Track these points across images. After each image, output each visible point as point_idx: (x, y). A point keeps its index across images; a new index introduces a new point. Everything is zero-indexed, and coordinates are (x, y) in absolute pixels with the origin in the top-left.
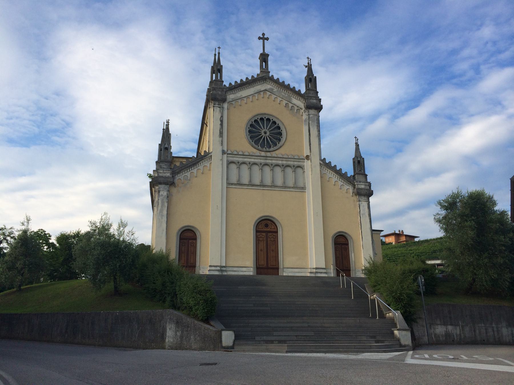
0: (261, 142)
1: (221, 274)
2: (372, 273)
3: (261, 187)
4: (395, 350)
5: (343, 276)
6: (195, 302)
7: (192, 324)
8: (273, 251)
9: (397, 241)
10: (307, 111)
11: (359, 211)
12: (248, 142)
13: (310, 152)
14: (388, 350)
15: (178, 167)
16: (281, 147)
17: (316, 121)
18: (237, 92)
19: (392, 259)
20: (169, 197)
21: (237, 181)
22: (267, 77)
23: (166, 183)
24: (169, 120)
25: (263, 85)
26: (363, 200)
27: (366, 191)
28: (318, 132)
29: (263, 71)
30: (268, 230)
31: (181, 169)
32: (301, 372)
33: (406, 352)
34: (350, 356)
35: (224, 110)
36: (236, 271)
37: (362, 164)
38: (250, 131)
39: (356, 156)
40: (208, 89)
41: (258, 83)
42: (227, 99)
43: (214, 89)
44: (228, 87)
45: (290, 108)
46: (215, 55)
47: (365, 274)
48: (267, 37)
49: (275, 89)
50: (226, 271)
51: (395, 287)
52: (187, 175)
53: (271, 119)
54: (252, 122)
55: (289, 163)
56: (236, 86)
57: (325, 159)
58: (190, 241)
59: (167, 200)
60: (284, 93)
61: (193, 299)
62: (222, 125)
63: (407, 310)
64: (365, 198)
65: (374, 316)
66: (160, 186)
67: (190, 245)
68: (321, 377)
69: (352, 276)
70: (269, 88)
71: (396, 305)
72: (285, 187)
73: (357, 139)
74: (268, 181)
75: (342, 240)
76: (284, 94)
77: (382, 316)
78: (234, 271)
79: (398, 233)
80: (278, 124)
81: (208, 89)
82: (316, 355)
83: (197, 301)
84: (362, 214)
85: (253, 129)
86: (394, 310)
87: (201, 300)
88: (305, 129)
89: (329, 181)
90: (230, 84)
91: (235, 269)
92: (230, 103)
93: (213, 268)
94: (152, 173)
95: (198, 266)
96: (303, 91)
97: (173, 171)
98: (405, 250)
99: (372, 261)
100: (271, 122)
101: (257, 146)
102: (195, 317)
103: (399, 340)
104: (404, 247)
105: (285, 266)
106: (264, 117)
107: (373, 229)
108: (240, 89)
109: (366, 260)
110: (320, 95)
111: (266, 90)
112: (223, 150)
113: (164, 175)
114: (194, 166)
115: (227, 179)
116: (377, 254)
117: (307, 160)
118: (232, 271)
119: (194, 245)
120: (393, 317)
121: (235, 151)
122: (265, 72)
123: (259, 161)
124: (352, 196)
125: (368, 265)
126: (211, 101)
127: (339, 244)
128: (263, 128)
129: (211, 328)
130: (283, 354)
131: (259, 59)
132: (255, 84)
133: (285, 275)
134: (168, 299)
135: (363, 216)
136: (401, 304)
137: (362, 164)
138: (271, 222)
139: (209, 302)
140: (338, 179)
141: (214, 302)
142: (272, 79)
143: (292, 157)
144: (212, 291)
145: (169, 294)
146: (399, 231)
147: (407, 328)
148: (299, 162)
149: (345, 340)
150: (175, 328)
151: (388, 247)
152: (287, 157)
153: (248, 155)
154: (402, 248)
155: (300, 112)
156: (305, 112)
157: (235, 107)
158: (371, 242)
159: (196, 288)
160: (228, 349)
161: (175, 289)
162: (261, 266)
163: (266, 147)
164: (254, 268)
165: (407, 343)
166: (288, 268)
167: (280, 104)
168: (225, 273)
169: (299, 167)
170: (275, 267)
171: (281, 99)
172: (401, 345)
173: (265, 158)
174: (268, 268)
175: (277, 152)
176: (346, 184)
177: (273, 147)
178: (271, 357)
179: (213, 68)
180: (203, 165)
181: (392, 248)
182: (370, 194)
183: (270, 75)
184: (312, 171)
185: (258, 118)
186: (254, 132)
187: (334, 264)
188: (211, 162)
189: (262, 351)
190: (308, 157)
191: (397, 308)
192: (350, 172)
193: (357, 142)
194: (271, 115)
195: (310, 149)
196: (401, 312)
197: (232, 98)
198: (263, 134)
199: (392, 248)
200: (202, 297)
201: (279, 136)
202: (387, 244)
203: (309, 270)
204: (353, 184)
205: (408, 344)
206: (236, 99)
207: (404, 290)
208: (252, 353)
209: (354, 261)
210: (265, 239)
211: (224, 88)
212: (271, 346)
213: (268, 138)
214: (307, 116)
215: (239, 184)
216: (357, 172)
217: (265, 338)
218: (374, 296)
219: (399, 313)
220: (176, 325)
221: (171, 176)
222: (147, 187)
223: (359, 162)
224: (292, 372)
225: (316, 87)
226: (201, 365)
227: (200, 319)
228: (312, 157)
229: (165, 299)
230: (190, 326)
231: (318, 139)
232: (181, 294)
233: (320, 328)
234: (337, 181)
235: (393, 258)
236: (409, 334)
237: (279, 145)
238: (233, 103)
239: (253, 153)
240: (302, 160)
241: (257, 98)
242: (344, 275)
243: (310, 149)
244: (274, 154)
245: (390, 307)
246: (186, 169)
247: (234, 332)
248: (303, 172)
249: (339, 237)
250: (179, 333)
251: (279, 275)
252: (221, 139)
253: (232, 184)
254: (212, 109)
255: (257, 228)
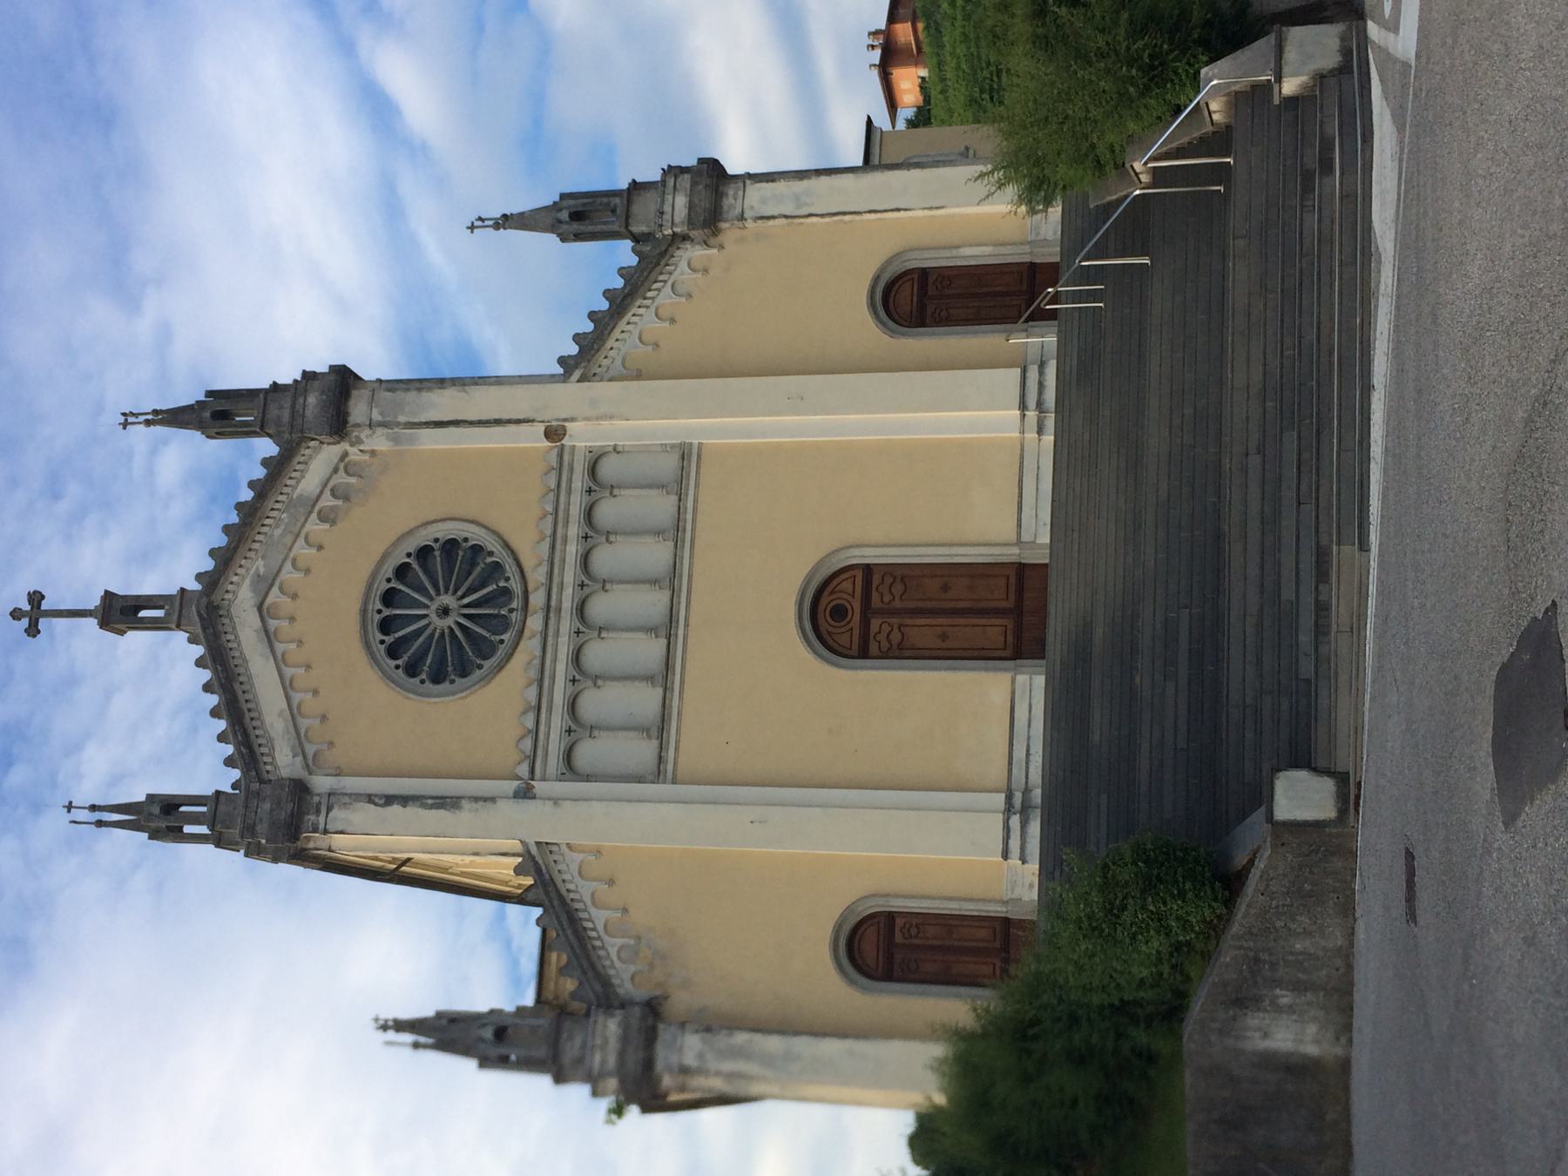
0: (484, 633)
1: (1038, 812)
2: (1044, 176)
3: (676, 635)
4: (1361, 96)
5: (1056, 299)
6: (1152, 932)
7: (1244, 943)
8: (945, 588)
9: (914, 57)
10: (354, 434)
11: (784, 221)
12: (482, 687)
13: (533, 421)
14: (1363, 126)
15: (581, 983)
16: (507, 546)
17: (399, 392)
18: (266, 731)
19: (988, 81)
20: (711, 1024)
21: (649, 737)
22: (204, 600)
23: (650, 1038)
24: (376, 1020)
25: (236, 620)
26: (740, 201)
27: (701, 187)
28: (445, 385)
29: (175, 617)
30: (857, 605)
31: (590, 974)
32: (1446, 498)
33: (1370, 51)
34: (1382, 287)
35: (344, 788)
36: (1028, 750)
37: (586, 201)
38: (438, 677)
39: (553, 226)
40: (246, 855)
41: (228, 641)
42: (295, 776)
43: (249, 829)
44: (242, 772)
45: (340, 502)
46: (100, 824)
47: (1048, 202)
48: (39, 632)
49: (254, 569)
50: (1027, 791)
51: (1102, 83)
52: (616, 949)
53: (386, 586)
54: (397, 667)
55: (576, 510)
56: (240, 738)
57: (562, 361)
58: (898, 938)
59: (724, 1032)
60: (275, 527)
61: (1140, 937)
62: (404, 800)
63: (1196, 36)
64: (731, 192)
65: (1221, 173)
66: (660, 1065)
67: (916, 941)
68: (1467, 419)
69: (1058, 259)
70: (252, 595)
71: (1176, 81)
72: (677, 531)
73: (479, 223)
74: (652, 603)
75: (906, 297)
76: (277, 526)
77: (1219, 140)
78: (1028, 754)
79: (877, 53)
80: (409, 555)
81: (246, 855)
82: (1377, 427)
83: (1148, 924)
84: (799, 207)
85: (428, 662)
86: (1198, 92)
87: (1143, 908)
88: (431, 441)
89: (657, 345)
90: (229, 762)
91: (1019, 753)
92: (310, 762)
93: (1015, 844)
94: (605, 1103)
95: (1005, 909)
96: (266, 447)
97: (599, 1006)
98: (953, 25)
99: (992, 172)
100: (401, 587)
101: (501, 651)
102: (1214, 930)
103: (1321, 78)
104: (938, 31)
105: (1013, 537)
106: (377, 617)
107: (861, 165)
108: (252, 719)
109: (988, 197)
110: (288, 375)
111: (260, 608)
112: (515, 797)
113: (613, 1044)
114: (581, 919)
115: (639, 782)
116: (967, 149)
117: (565, 434)
118: (1027, 763)
119: (914, 922)
120: (1228, 94)
121: (521, 746)
122: (180, 611)
123: (564, 640)
124: (722, 247)
125: (1011, 191)
126: (299, 844)
127: (922, 307)
128: (423, 623)
129: (1261, 864)
130: (1372, 563)
131: (122, 633)
132: (232, 653)
133: (1049, 537)
134: (1141, 1037)
135: (806, 204)
136: (1173, 61)
137: (586, 201)
138: (826, 593)
139: (1155, 872)
140: (647, 307)
141: (1153, 850)
142: (210, 581)
143: (551, 496)
144: (1107, 856)
145: (1119, 1036)
146: (873, 47)
147: (1273, 41)
148: (571, 469)
149: (1319, 298)
150: (1261, 1015)
151: (940, 96)
152: (550, 519)
153: (541, 687)
154: (944, 39)
155: (356, 463)
156: (359, 441)
157: (331, 744)
158: (916, 173)
159: (1094, 924)
160: (1348, 796)
161: (1101, 1007)
162: (1010, 639)
163: (506, 609)
164: (1016, 671)
165: (1334, 44)
166: (1019, 525)
167: (320, 548)
168: (1037, 795)
169: (593, 470)
170: (1013, 581)
171: (301, 541)
172: (1343, 70)
173: (552, 615)
174: (1018, 611)
175: (528, 562)
176: (670, 273)
177: (507, 579)
178: (1383, 619)
179: (155, 835)
180: (578, 879)
181: (943, 80)
182: (711, 173)
183: (193, 586)
184: (611, 417)
185: (382, 642)
186: (441, 662)
187: (1003, 332)
188: (564, 848)
189: (1360, 653)
190: (554, 433)
191: (1187, 76)
192: (623, 253)
193: (491, 223)
194: (370, 586)
195: (518, 422)
196: (1207, 64)
197: (291, 755)
198: (449, 622)
199: (943, 80)
200: (1130, 900)
201: (461, 553)
202: (924, 100)
203: (1031, 435)
204: (669, 246)
205: (1338, 41)
206: (295, 735)
207: (1115, 50)
208: (1368, 697)
209: (995, 245)
210: (895, 621)
211: (248, 789)
212: (1340, 614)
213: (466, 601)
214: (374, 433)
215: (660, 728)
216: (618, 223)
217: (1305, 638)
218: (1138, 171)
219: (1210, 70)
220: (1247, 1008)
221: (618, 1012)
222: (659, 1120)
223: (577, 216)
224: (1445, 536)
225: (251, 394)
226: (1412, 915)
227: (1225, 911)
228: (553, 414)
229: (1140, 1055)
230: (1251, 954)
231: (472, 387)
232: (1118, 985)
233: (1269, 404)
234: (657, 309)
235: (985, 78)
236: (1297, 35)
237: (500, 555)
238: (310, 749)
239: (529, 664)
240: (566, 458)
241: (293, 646)
242: (1050, 290)
243: (518, 422)
244: (537, 576)
245: (1186, 108)
246: (592, 953)
247: (1281, 771)
248: (614, 456)
249: (891, 305)
250: (1283, 996)
251: (1047, 561)
252: (464, 803)
253: (661, 759)
254: (338, 841)
255: (848, 652)
